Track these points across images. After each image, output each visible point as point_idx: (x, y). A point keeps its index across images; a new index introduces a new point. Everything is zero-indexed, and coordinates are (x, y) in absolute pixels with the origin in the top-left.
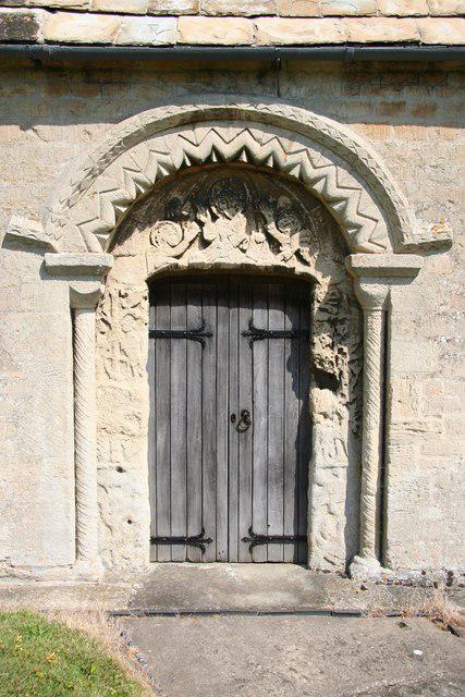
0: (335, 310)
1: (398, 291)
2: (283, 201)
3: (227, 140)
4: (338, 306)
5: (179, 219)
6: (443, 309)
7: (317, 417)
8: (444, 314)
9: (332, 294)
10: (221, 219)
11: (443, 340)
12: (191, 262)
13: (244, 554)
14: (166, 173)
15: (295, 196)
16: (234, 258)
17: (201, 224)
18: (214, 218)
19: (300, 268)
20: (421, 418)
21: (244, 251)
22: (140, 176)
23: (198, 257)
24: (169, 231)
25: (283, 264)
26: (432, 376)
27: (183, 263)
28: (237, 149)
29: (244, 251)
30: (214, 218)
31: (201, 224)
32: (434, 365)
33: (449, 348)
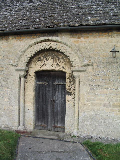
0: (70, 79)
1: (82, 74)
2: (60, 57)
3: (47, 45)
4: (71, 78)
5: (40, 60)
6: (91, 79)
7: (67, 101)
8: (91, 80)
9: (70, 76)
10: (48, 61)
11: (91, 85)
12: (110, 39)
13: (53, 129)
14: (46, 49)
15: (62, 56)
16: (50, 68)
17: (45, 61)
18: (47, 60)
19: (64, 70)
20: (86, 102)
21: (53, 67)
22: (32, 53)
23: (44, 68)
24: (39, 63)
25: (60, 69)
26: (89, 93)
27: (41, 69)
28: (50, 46)
29: (53, 67)
30: (47, 60)
31: (45, 61)
32: (89, 91)
33: (92, 87)
